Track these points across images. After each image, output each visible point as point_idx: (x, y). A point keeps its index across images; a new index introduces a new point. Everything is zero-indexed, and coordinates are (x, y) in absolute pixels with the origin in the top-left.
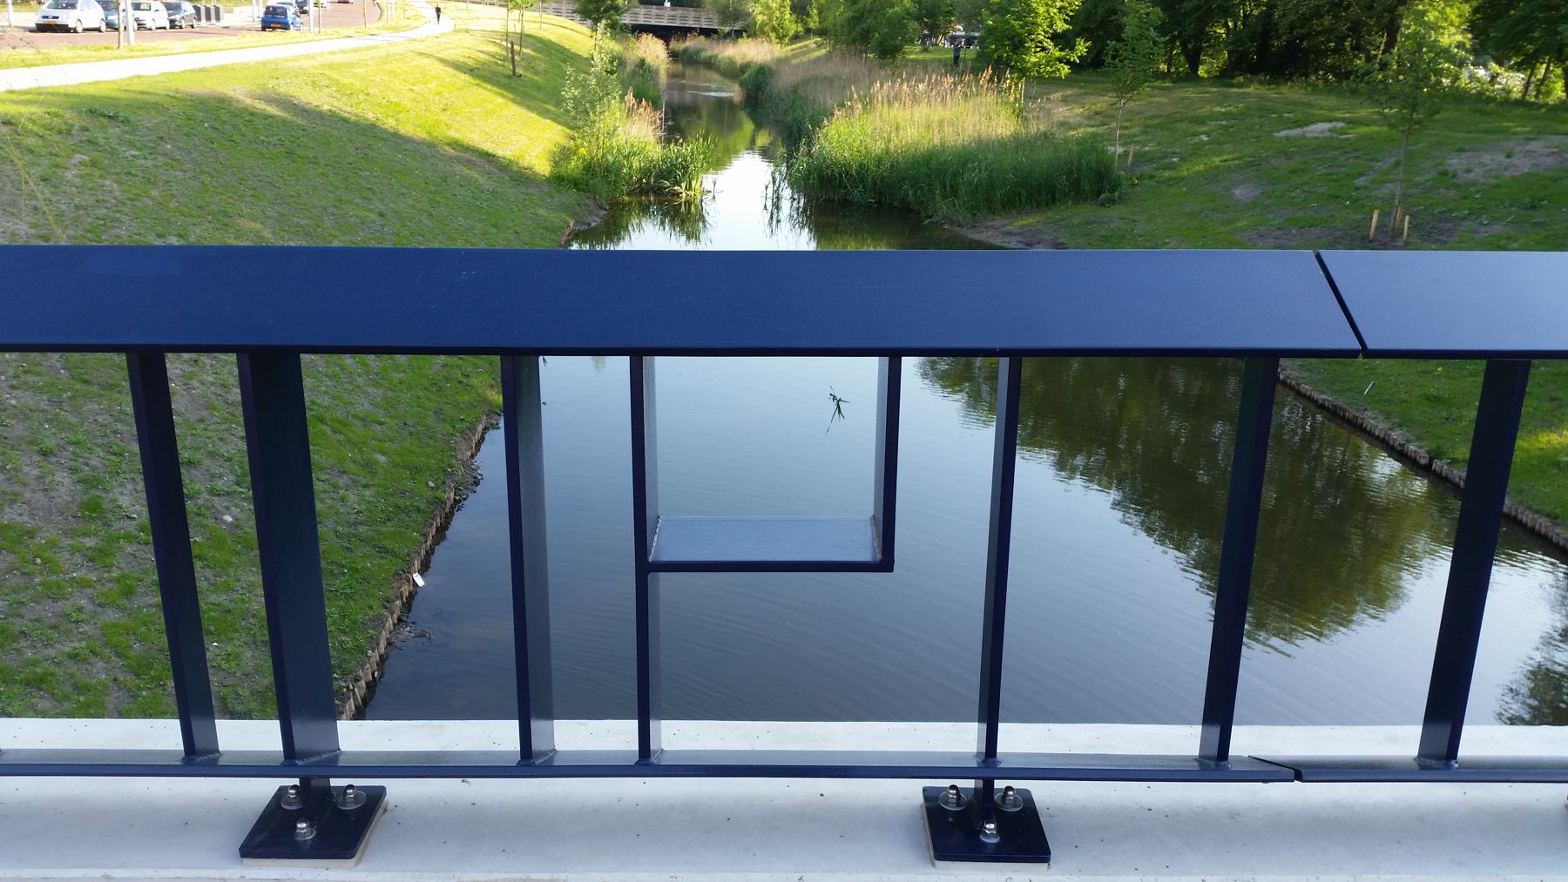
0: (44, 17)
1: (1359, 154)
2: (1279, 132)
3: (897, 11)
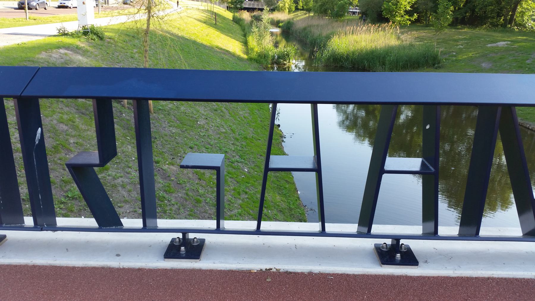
0: (61, 3)
1: (522, 52)
2: (487, 45)
3: (342, 3)
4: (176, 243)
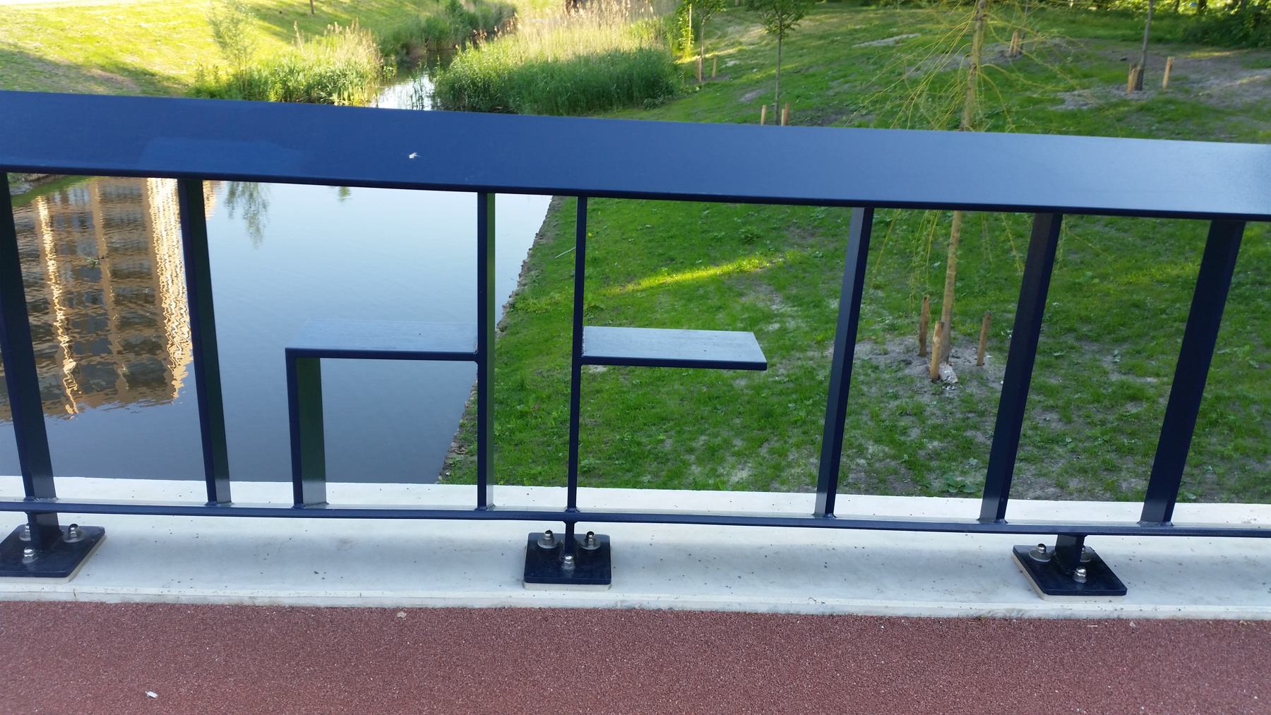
4: (24, 537)
